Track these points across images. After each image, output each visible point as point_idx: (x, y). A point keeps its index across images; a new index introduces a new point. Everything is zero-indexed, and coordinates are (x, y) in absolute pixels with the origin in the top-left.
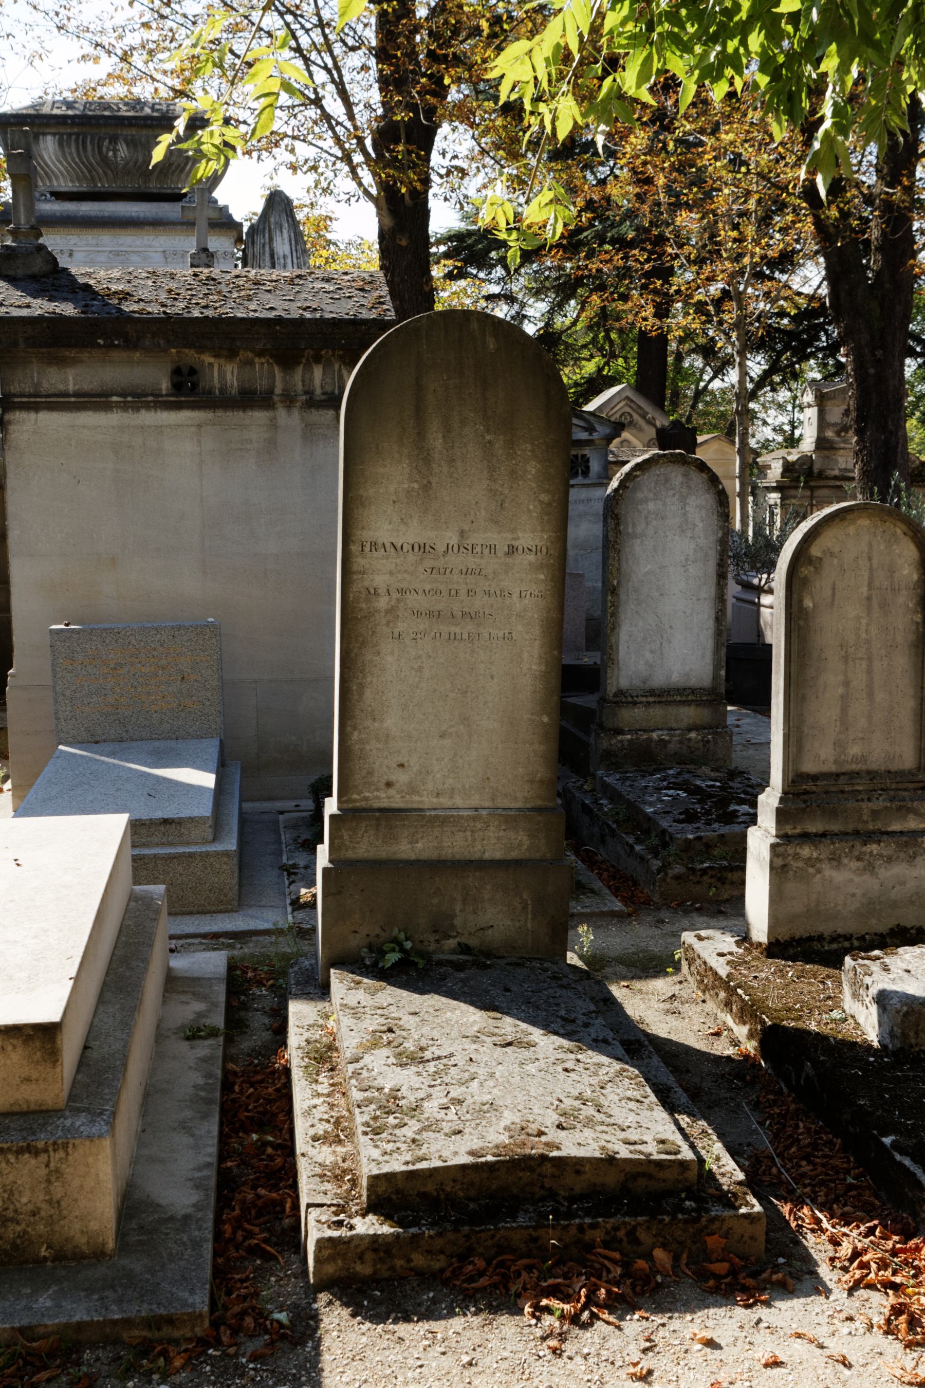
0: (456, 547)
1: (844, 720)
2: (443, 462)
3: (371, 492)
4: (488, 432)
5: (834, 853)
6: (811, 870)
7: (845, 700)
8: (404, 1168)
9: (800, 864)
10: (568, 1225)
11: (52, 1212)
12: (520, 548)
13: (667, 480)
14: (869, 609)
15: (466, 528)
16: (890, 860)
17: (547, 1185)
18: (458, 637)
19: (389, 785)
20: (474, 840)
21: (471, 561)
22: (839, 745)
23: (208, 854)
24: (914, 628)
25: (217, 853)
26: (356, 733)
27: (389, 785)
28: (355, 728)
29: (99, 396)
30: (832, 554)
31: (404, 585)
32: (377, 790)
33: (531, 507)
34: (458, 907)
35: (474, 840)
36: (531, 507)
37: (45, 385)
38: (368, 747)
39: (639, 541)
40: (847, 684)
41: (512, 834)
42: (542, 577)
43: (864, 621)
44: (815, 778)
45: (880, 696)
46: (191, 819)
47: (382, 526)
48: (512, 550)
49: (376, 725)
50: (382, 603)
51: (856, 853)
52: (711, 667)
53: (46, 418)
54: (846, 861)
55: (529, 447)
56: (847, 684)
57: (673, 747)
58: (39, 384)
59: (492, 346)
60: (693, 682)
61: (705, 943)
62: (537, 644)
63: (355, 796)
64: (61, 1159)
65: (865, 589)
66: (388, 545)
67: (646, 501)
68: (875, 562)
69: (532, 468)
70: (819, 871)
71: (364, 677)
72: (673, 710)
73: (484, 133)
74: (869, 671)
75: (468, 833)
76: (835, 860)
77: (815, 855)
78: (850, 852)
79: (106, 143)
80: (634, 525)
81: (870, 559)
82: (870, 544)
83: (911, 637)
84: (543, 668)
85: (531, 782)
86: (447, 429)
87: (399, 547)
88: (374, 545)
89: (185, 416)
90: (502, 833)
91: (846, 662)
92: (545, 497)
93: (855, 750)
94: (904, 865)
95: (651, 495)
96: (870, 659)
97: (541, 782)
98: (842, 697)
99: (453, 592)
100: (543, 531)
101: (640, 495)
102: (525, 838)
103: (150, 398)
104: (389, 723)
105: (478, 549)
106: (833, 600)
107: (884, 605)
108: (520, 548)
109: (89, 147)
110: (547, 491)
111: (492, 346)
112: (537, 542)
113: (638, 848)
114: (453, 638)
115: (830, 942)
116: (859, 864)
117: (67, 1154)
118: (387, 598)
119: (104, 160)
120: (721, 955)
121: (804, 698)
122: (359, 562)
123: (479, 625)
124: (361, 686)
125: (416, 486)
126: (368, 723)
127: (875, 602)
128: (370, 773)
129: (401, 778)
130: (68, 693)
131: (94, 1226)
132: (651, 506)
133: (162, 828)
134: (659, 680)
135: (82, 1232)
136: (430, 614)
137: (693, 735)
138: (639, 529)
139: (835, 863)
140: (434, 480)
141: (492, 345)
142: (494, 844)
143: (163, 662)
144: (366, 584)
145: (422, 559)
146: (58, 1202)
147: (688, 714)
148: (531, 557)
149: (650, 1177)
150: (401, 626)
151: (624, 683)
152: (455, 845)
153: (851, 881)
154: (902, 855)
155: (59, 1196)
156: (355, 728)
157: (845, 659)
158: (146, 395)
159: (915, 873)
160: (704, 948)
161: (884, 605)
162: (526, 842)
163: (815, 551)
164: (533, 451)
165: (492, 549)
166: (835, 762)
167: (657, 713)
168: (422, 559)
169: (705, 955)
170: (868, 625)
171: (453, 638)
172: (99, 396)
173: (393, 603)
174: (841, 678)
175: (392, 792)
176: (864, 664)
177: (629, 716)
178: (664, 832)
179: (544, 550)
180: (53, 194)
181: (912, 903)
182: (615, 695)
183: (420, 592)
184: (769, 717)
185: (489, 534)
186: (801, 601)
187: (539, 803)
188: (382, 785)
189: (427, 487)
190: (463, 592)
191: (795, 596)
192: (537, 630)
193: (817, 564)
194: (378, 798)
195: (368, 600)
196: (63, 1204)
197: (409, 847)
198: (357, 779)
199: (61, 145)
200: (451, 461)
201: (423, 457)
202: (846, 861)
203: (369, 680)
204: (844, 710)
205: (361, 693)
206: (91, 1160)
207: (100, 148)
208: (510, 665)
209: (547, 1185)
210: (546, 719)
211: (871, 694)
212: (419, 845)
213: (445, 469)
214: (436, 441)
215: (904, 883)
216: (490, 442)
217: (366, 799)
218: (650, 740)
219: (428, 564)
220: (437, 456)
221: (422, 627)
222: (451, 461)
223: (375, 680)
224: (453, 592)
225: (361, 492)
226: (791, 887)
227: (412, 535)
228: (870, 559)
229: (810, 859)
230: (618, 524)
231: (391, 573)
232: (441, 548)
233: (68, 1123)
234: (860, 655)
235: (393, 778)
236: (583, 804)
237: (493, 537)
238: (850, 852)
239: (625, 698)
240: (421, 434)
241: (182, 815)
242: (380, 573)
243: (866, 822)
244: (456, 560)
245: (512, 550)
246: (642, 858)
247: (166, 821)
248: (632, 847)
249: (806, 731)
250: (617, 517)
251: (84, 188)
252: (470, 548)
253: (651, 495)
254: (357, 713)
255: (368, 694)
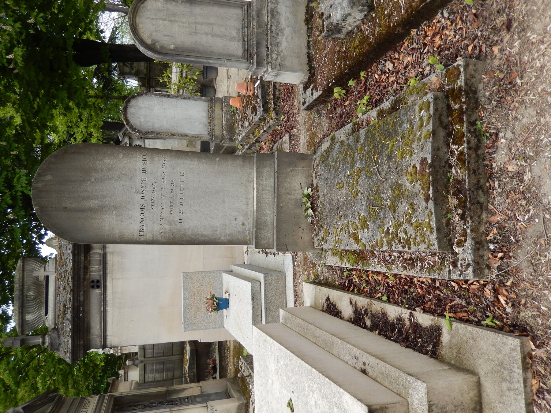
0: (142, 195)
1: (222, 36)
2: (104, 200)
3: (117, 232)
4: (90, 180)
5: (275, 45)
6: (282, 54)
7: (214, 35)
8: (435, 234)
9: (279, 58)
10: (468, 155)
11: (459, 409)
12: (143, 167)
13: (133, 114)
14: (175, 21)
15: (134, 191)
16: (278, 22)
17: (444, 164)
18: (182, 195)
19: (243, 224)
20: (266, 190)
21: (148, 189)
22: (232, 39)
23: (265, 284)
24: (184, 3)
25: (265, 281)
26: (222, 238)
27: (243, 224)
28: (220, 238)
29: (101, 314)
30: (151, 35)
31: (159, 217)
32: (245, 229)
33: (125, 162)
34: (293, 197)
35: (266, 190)
36: (125, 162)
37: (97, 333)
38: (228, 233)
39: (155, 125)
40: (207, 34)
41: (264, 175)
42: (156, 158)
43: (180, 24)
44: (244, 50)
45: (212, 20)
46: (252, 290)
47: (132, 227)
48: (144, 171)
49: (218, 229)
50: (167, 227)
51: (275, 36)
52: (201, 102)
53: (109, 333)
54: (278, 40)
55: (98, 162)
56: (207, 34)
57: (229, 117)
58: (97, 335)
59: (50, 177)
60: (206, 108)
61: (307, 100)
62: (186, 161)
63: (248, 238)
64: (436, 408)
65: (166, 22)
66: (141, 224)
67: (140, 122)
68: (154, 17)
69: (108, 161)
70: (282, 51)
71: (198, 234)
72: (216, 116)
73: (487, 165)
74: (201, 24)
75: (264, 192)
76: (278, 44)
77: (276, 52)
78: (275, 38)
79: (28, 299)
80: (149, 126)
81: (153, 19)
82: (147, 18)
83: (188, 5)
84: (196, 159)
85: (243, 166)
86: (88, 198)
87: (142, 220)
88: (140, 231)
89: (109, 284)
90: (264, 179)
91: (197, 33)
92: (121, 156)
93: (234, 33)
94: (281, 16)
95: (138, 120)
96: (196, 23)
97: (243, 162)
98: (212, 36)
99: (162, 197)
100: (136, 157)
101: (138, 124)
102: (266, 169)
103: (102, 296)
104: (218, 225)
105: (143, 185)
106: (171, 36)
107: (174, 15)
108: (143, 167)
109: (30, 304)
110: (118, 155)
111: (50, 177)
112: (141, 160)
113: (265, 129)
114: (182, 197)
115: (310, 49)
116: (280, 34)
117: (434, 404)
118: (164, 225)
119: (34, 299)
120: (312, 94)
121: (212, 52)
122: (149, 237)
123: (177, 186)
124: (202, 236)
125: (114, 212)
126: (218, 232)
127: (173, 19)
128: (239, 232)
129: (241, 219)
130: (206, 325)
131: (465, 387)
132: (142, 120)
133: (255, 300)
134: (205, 121)
135: (469, 393)
136: (171, 207)
137: (224, 109)
138: (151, 125)
139: (279, 44)
140: (112, 204)
141: (49, 177)
142: (270, 182)
143: (196, 292)
144: (158, 234)
145: (148, 210)
146: (455, 406)
147: (217, 111)
148: (148, 163)
149: (441, 115)
150: (177, 219)
151: (206, 133)
152: (269, 198)
153: (286, 39)
154: (277, 17)
155: (453, 406)
156: (220, 238)
157: (196, 33)
158: (101, 298)
159: (284, 13)
160: (309, 100)
161: (174, 15)
162: (268, 169)
163: (149, 42)
164: (100, 160)
165: (143, 179)
166: (238, 41)
167: (217, 122)
168: (148, 210)
169: (312, 100)
170: (181, 22)
171: (182, 197)
172: (101, 314)
173: (167, 222)
174: (204, 36)
175: (246, 223)
176: (199, 26)
177: (217, 132)
178: (260, 119)
179: (144, 157)
180: (46, 315)
181: (295, 15)
182: (210, 136)
183: (162, 211)
184: (212, 343)
185: (137, 180)
186: (171, 50)
187: (252, 163)
188: (244, 227)
189: (115, 207)
190: (162, 192)
191: (168, 52)
192: (180, 161)
193: (154, 43)
194: (248, 229)
195: (165, 233)
196: (456, 404)
197: (270, 216)
198: (241, 237)
199: (29, 313)
200: (104, 196)
201: (101, 209)
202: (278, 40)
203: (200, 233)
204: (217, 36)
205: (206, 236)
206: (436, 392)
207: (29, 301)
208: (199, 174)
209: (444, 164)
210: (218, 159)
211: (211, 24)
212: (268, 212)
213: (107, 199)
214: (94, 203)
215: (288, 18)
216: (95, 179)
217: (249, 233)
218: (226, 124)
219: (150, 207)
220: (101, 203)
221: (178, 210)
222: (104, 196)
223: (200, 230)
224: (162, 197)
225: (117, 236)
226: (288, 63)
227: (136, 213)
228: (153, 19)
229: (277, 55)
230: (149, 132)
231: (154, 223)
232: (142, 202)
233: (416, 402)
234: (194, 27)
235: (241, 223)
236: (248, 149)
237: (138, 179)
238: (275, 38)
239: (212, 134)
240: (91, 210)
241: (251, 293)
242: (153, 228)
243: (263, 31)
244: (147, 196)
245: (144, 171)
246: (269, 127)
247: (253, 299)
248: (265, 131)
249: (225, 52)
250: (146, 133)
251: (44, 305)
252: (143, 189)
253: (138, 120)
254: (213, 237)
255: (205, 233)
